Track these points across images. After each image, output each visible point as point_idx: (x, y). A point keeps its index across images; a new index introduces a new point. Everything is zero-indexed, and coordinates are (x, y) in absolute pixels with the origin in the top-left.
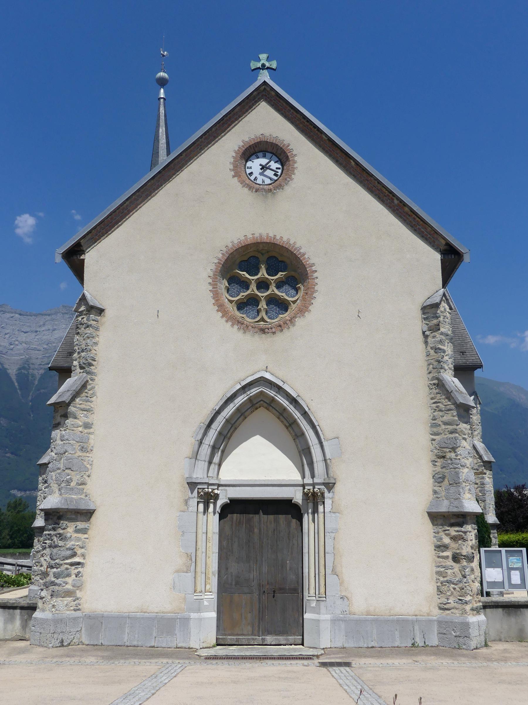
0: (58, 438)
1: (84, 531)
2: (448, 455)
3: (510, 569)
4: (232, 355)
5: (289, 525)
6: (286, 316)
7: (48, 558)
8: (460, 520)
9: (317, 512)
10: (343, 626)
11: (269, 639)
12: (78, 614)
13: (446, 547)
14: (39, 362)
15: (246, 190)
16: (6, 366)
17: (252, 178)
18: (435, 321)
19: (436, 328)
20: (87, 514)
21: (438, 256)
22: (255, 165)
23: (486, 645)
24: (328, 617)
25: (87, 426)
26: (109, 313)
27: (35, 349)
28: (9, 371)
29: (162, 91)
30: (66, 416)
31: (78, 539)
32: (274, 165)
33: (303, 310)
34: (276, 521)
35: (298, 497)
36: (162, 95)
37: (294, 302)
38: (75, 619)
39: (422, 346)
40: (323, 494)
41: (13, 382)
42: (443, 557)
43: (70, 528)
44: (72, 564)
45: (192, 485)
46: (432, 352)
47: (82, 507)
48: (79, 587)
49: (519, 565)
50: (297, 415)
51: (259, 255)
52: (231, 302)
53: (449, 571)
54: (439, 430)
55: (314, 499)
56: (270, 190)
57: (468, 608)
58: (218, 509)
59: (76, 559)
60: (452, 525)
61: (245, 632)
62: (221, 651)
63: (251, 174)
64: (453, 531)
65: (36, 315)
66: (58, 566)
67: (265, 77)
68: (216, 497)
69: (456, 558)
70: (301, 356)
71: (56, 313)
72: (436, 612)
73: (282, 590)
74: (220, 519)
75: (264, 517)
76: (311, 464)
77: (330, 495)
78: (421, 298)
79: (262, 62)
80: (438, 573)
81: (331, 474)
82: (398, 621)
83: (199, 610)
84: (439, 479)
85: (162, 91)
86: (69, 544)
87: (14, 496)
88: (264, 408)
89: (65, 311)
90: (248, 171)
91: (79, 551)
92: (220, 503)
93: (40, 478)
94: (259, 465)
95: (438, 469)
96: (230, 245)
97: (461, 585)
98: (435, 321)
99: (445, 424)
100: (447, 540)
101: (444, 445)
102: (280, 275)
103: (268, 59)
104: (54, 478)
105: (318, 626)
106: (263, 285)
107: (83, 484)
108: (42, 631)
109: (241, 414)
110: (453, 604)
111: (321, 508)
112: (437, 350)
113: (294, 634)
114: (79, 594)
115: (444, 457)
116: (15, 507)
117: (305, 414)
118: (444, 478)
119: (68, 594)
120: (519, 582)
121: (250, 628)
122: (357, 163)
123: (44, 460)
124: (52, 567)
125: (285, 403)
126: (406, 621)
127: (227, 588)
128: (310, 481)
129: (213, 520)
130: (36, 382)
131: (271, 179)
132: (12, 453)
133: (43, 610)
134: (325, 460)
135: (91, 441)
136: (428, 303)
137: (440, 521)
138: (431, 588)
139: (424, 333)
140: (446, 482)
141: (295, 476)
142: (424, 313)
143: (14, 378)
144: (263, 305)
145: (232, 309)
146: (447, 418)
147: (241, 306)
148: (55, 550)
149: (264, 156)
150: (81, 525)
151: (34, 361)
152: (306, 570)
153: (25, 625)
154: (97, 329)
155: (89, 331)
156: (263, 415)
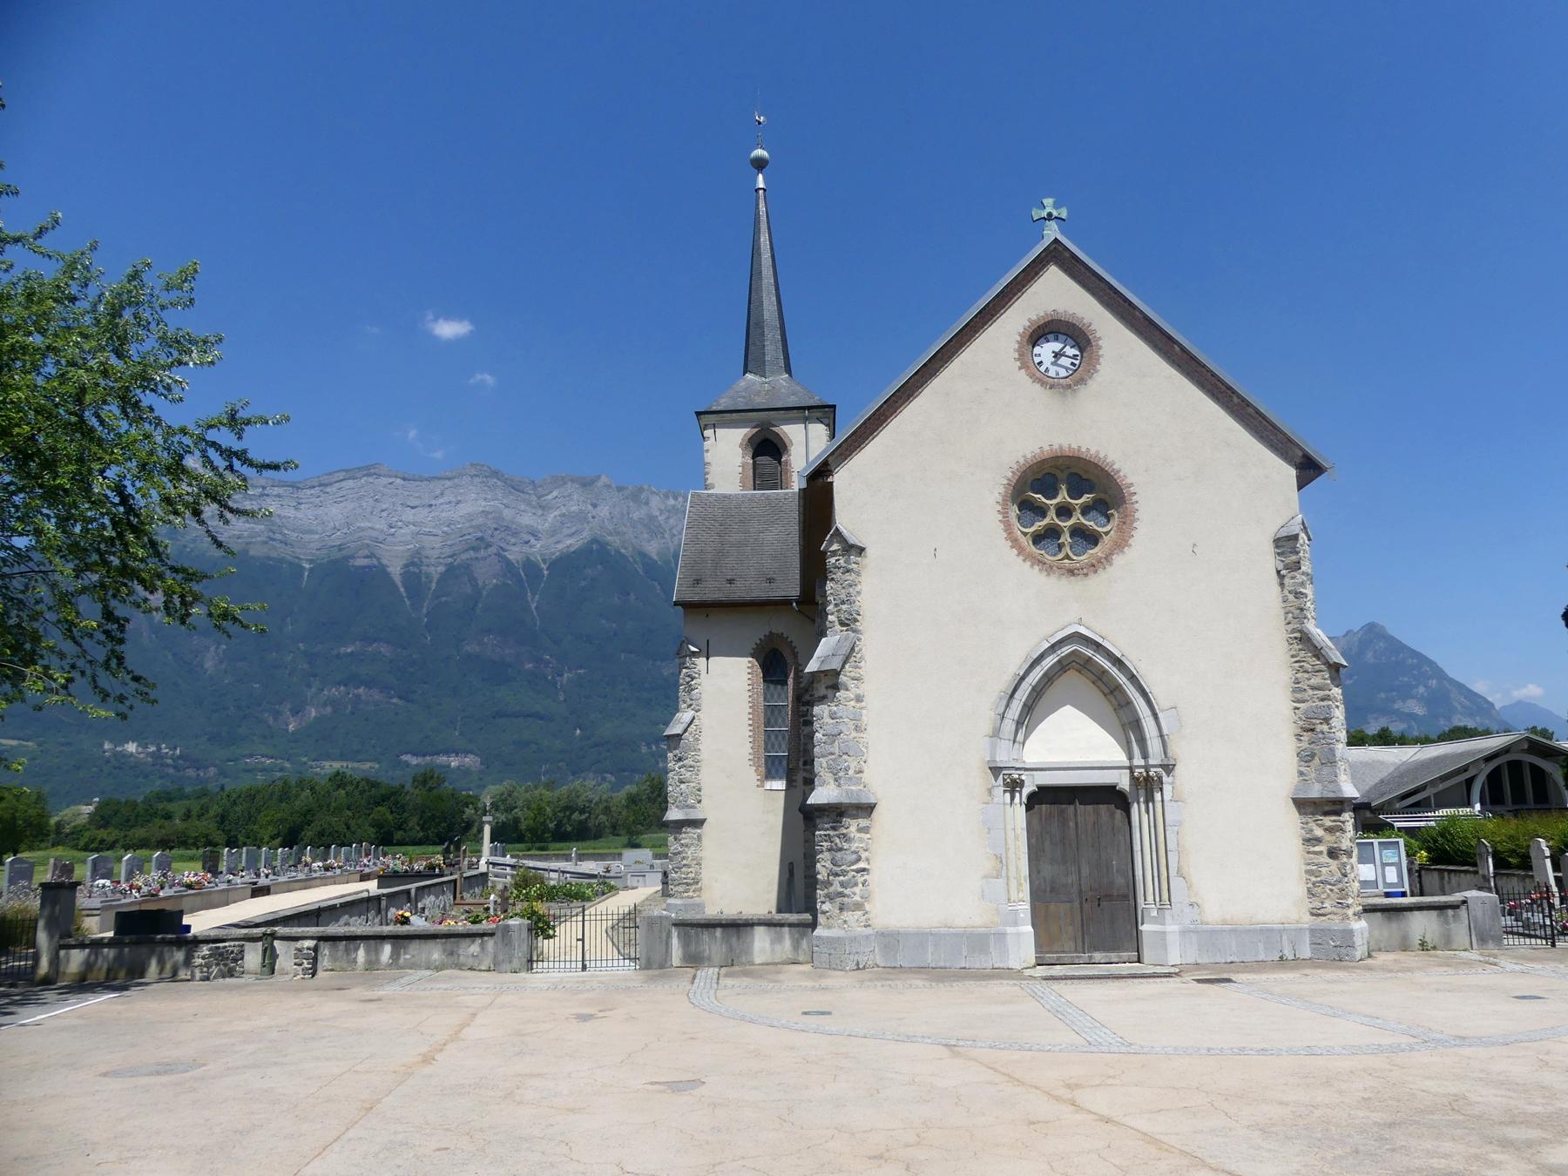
0: (826, 714)
1: (865, 830)
2: (1319, 728)
3: (1384, 865)
4: (1037, 606)
5: (1112, 815)
6: (1097, 551)
7: (829, 864)
8: (1338, 807)
11: (1098, 956)
12: (869, 931)
13: (1318, 840)
14: (435, 553)
15: (1037, 386)
16: (384, 562)
17: (1042, 369)
18: (1294, 558)
19: (1296, 566)
20: (867, 809)
21: (1293, 472)
22: (1046, 350)
23: (1370, 956)
24: (1176, 928)
25: (859, 699)
27: (429, 534)
28: (390, 569)
30: (836, 687)
31: (861, 840)
32: (1070, 351)
33: (1121, 545)
34: (1097, 814)
35: (1124, 782)
36: (761, 184)
37: (1107, 533)
38: (867, 937)
40: (1160, 779)
41: (396, 586)
43: (852, 826)
44: (858, 871)
45: (996, 770)
46: (1291, 597)
47: (864, 801)
48: (865, 898)
49: (1396, 860)
50: (1122, 679)
52: (1025, 534)
53: (1324, 870)
54: (1305, 696)
55: (1148, 785)
56: (1069, 386)
57: (1350, 912)
58: (1024, 799)
59: (861, 865)
60: (1326, 814)
61: (801, 959)
62: (1041, 971)
63: (1040, 363)
64: (1328, 821)
65: (429, 480)
66: (844, 873)
67: (1052, 232)
68: (1021, 784)
69: (1333, 853)
70: (1120, 602)
71: (461, 475)
72: (1307, 918)
73: (1109, 897)
74: (1028, 809)
75: (1081, 808)
76: (1142, 741)
77: (1170, 779)
78: (1273, 526)
79: (1048, 210)
80: (1307, 872)
81: (1170, 754)
83: (1016, 924)
84: (1306, 757)
86: (854, 846)
87: (407, 764)
88: (1084, 672)
89: (473, 472)
90: (1037, 360)
91: (864, 855)
92: (1026, 791)
94: (1075, 744)
95: (1305, 745)
96: (1022, 461)
98: (1294, 558)
99: (1313, 688)
100: (1319, 832)
102: (1086, 498)
103: (1056, 206)
105: (1164, 939)
106: (1065, 512)
107: (861, 772)
109: (1049, 679)
110: (1329, 909)
111: (1158, 796)
112: (1298, 595)
114: (867, 907)
116: (425, 782)
117: (1133, 678)
118: (1313, 756)
119: (858, 906)
120: (1395, 880)
121: (1072, 944)
122: (1183, 349)
123: (675, 729)
124: (837, 875)
125: (1106, 665)
126: (1272, 930)
127: (1043, 896)
128: (1142, 763)
129: (1021, 811)
130: (433, 586)
131: (1067, 369)
132: (400, 698)
133: (829, 927)
134: (1162, 736)
135: (864, 718)
136: (1283, 533)
138: (1301, 890)
141: (1120, 757)
142: (1277, 547)
143: (398, 580)
144: (1066, 538)
145: (1026, 542)
146: (1315, 681)
147: (1037, 539)
148: (839, 855)
149: (1056, 339)
150: (863, 822)
151: (428, 552)
152: (1139, 873)
153: (796, 946)
154: (858, 574)
155: (850, 577)
156: (1072, 677)
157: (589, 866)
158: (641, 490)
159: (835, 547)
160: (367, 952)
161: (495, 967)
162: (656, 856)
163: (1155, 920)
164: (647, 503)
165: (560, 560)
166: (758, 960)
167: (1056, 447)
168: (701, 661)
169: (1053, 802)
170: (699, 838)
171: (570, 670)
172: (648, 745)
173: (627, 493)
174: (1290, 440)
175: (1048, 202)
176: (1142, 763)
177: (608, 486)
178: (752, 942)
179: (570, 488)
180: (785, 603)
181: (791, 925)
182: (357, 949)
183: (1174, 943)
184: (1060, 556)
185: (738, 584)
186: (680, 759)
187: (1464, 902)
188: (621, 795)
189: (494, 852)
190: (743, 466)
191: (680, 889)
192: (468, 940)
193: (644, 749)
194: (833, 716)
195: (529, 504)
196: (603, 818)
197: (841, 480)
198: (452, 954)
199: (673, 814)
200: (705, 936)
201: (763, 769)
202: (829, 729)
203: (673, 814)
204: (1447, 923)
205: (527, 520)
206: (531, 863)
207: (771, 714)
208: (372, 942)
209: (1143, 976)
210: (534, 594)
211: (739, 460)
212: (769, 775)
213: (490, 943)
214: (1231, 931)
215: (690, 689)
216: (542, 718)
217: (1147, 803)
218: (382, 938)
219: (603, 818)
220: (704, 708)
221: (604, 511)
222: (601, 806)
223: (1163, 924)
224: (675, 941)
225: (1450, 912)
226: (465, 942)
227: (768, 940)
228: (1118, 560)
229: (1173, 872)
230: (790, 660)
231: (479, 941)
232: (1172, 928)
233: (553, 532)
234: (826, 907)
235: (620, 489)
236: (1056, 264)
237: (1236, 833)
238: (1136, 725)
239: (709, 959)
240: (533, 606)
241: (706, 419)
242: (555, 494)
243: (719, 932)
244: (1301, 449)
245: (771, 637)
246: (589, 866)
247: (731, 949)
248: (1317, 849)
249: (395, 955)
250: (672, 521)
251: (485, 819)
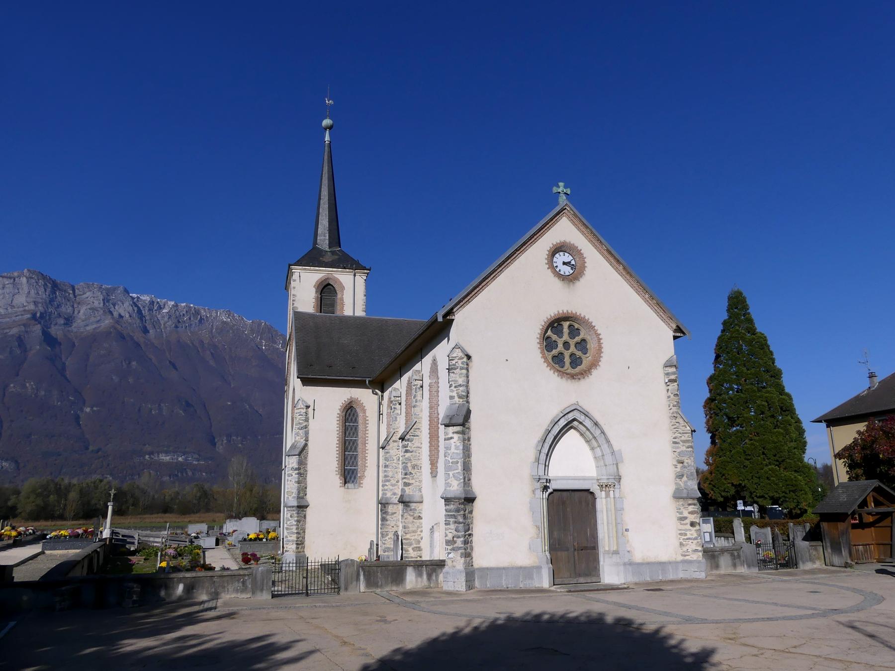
4: (554, 393)
7: (453, 531)
13: (686, 518)
22: (560, 258)
70: (593, 393)
90: (555, 265)
95: (678, 470)
103: (565, 187)
175: (561, 184)
216: (466, 542)
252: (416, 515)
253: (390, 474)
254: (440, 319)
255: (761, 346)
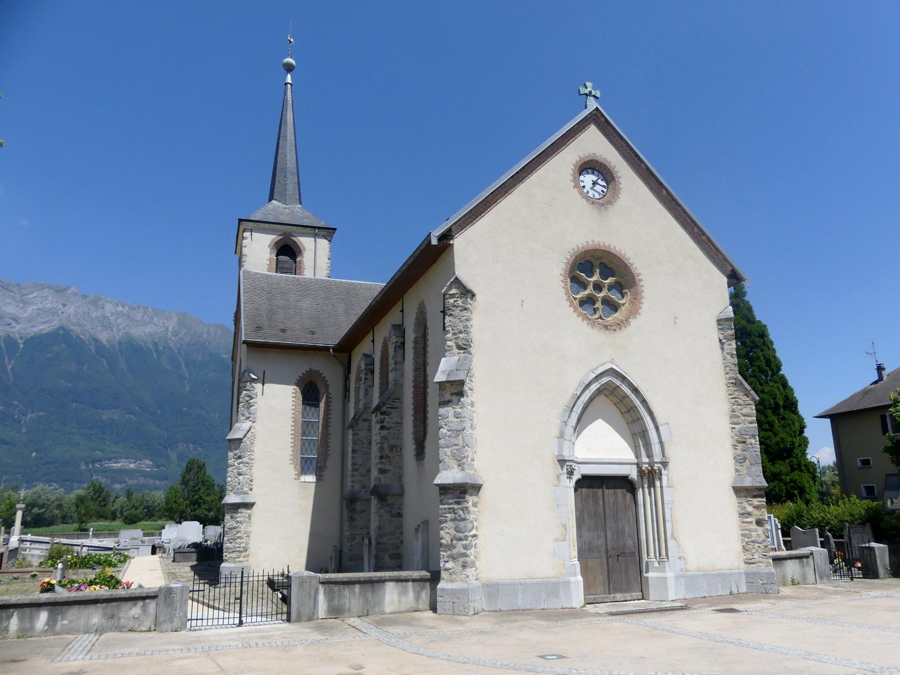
2: (749, 441)
5: (625, 496)
7: (452, 532)
9: (654, 487)
10: (683, 581)
11: (619, 596)
13: (749, 514)
17: (585, 191)
21: (725, 280)
22: (588, 179)
25: (472, 405)
26: (478, 297)
29: (289, 76)
32: (603, 183)
33: (634, 312)
34: (616, 495)
35: (633, 474)
37: (623, 305)
39: (720, 351)
42: (747, 522)
45: (562, 462)
50: (637, 403)
51: (594, 261)
52: (575, 299)
53: (753, 534)
54: (739, 420)
55: (651, 476)
56: (603, 205)
60: (754, 497)
63: (584, 187)
66: (466, 538)
72: (743, 565)
74: (576, 490)
75: (606, 491)
76: (648, 446)
80: (743, 535)
81: (666, 455)
82: (719, 575)
85: (289, 76)
88: (616, 398)
90: (582, 184)
93: (231, 454)
94: (605, 447)
97: (765, 544)
99: (744, 415)
101: (744, 432)
103: (594, 88)
104: (449, 453)
106: (598, 287)
108: (456, 600)
110: (758, 559)
111: (658, 483)
113: (635, 591)
114: (477, 564)
115: (744, 442)
117: (644, 401)
118: (745, 459)
121: (602, 588)
124: (460, 539)
125: (628, 392)
126: (725, 574)
133: (452, 581)
137: (743, 494)
138: (739, 548)
139: (720, 340)
140: (747, 462)
141: (630, 456)
142: (719, 325)
144: (598, 305)
148: (462, 524)
149: (593, 173)
152: (643, 537)
157: (108, 542)
158: (100, 299)
159: (453, 291)
160: (21, 620)
161: (156, 626)
162: (145, 535)
163: (657, 570)
164: (102, 308)
165: (33, 338)
166: (388, 610)
167: (596, 243)
168: (258, 386)
169: (589, 484)
170: (250, 517)
171: (33, 412)
172: (87, 464)
173: (88, 299)
174: (726, 260)
176: (647, 460)
177: (75, 294)
178: (384, 595)
179: (46, 292)
180: (326, 349)
181: (414, 580)
182: (9, 617)
183: (671, 583)
184: (596, 316)
185: (289, 333)
186: (240, 457)
187: (812, 554)
188: (73, 496)
189: (22, 533)
190: (270, 260)
191: (234, 555)
192: (130, 604)
193: (83, 467)
194: (457, 416)
195: (14, 298)
196: (56, 512)
197: (459, 242)
198: (112, 617)
199: (231, 498)
200: (346, 591)
201: (299, 467)
202: (454, 426)
203: (231, 498)
204: (804, 567)
205: (11, 309)
206: (64, 541)
207: (306, 427)
208: (28, 610)
209: (652, 611)
210: (10, 359)
211: (268, 256)
212: (304, 471)
213: (152, 605)
214: (704, 575)
215: (249, 406)
216: (7, 444)
217: (649, 487)
218: (39, 605)
219: (56, 512)
220: (258, 420)
221: (71, 309)
222: (56, 503)
223: (664, 572)
224: (321, 597)
225: (805, 560)
226: (126, 606)
227: (396, 592)
228: (633, 322)
229: (669, 536)
230: (322, 390)
231: (140, 603)
232: (670, 574)
233: (30, 319)
234: (448, 565)
235: (84, 297)
236: (595, 124)
237: (706, 507)
238: (644, 434)
239: (349, 610)
240: (9, 367)
241: (245, 225)
242: (35, 294)
243: (357, 588)
244: (731, 266)
245: (310, 371)
246: (108, 542)
247: (367, 601)
248: (748, 520)
249: (51, 622)
250: (119, 321)
251: (18, 506)
252: (395, 511)
253: (360, 462)
254: (434, 242)
255: (763, 334)
